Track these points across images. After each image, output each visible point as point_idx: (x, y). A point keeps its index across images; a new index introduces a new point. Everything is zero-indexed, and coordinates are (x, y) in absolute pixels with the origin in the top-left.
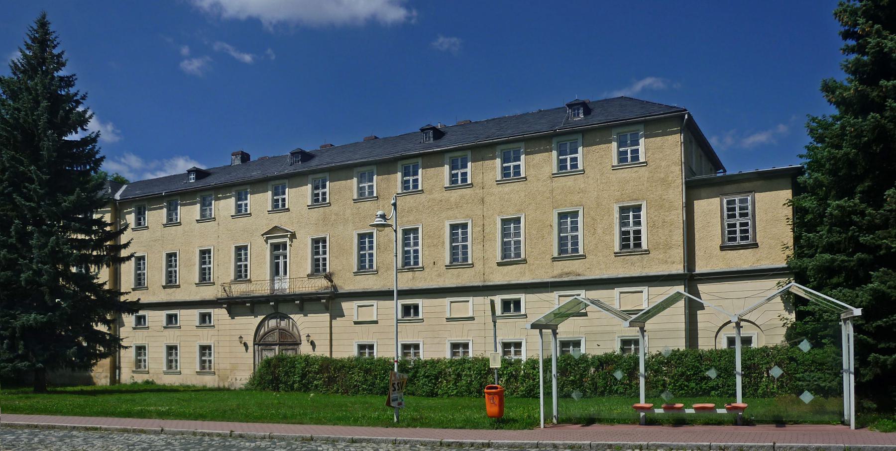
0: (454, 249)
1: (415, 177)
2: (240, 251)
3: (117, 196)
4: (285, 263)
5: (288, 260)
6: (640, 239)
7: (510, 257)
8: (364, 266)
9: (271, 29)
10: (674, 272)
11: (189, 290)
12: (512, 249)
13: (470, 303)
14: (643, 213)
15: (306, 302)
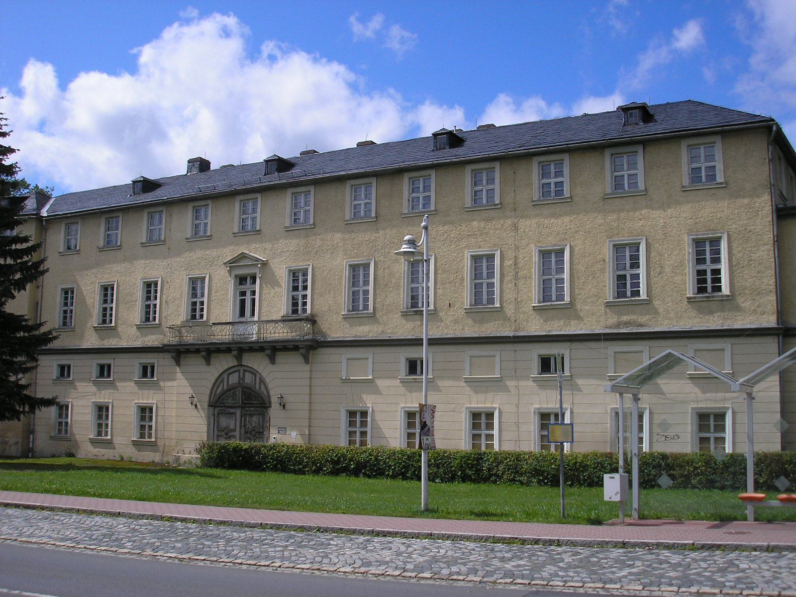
0: (477, 287)
1: (427, 194)
2: (196, 284)
3: (44, 213)
4: (253, 300)
5: (257, 297)
6: (719, 280)
7: (481, 304)
8: (357, 307)
9: (135, 51)
10: (765, 325)
11: (129, 334)
12: (554, 289)
13: (498, 359)
14: (724, 246)
15: (273, 350)
